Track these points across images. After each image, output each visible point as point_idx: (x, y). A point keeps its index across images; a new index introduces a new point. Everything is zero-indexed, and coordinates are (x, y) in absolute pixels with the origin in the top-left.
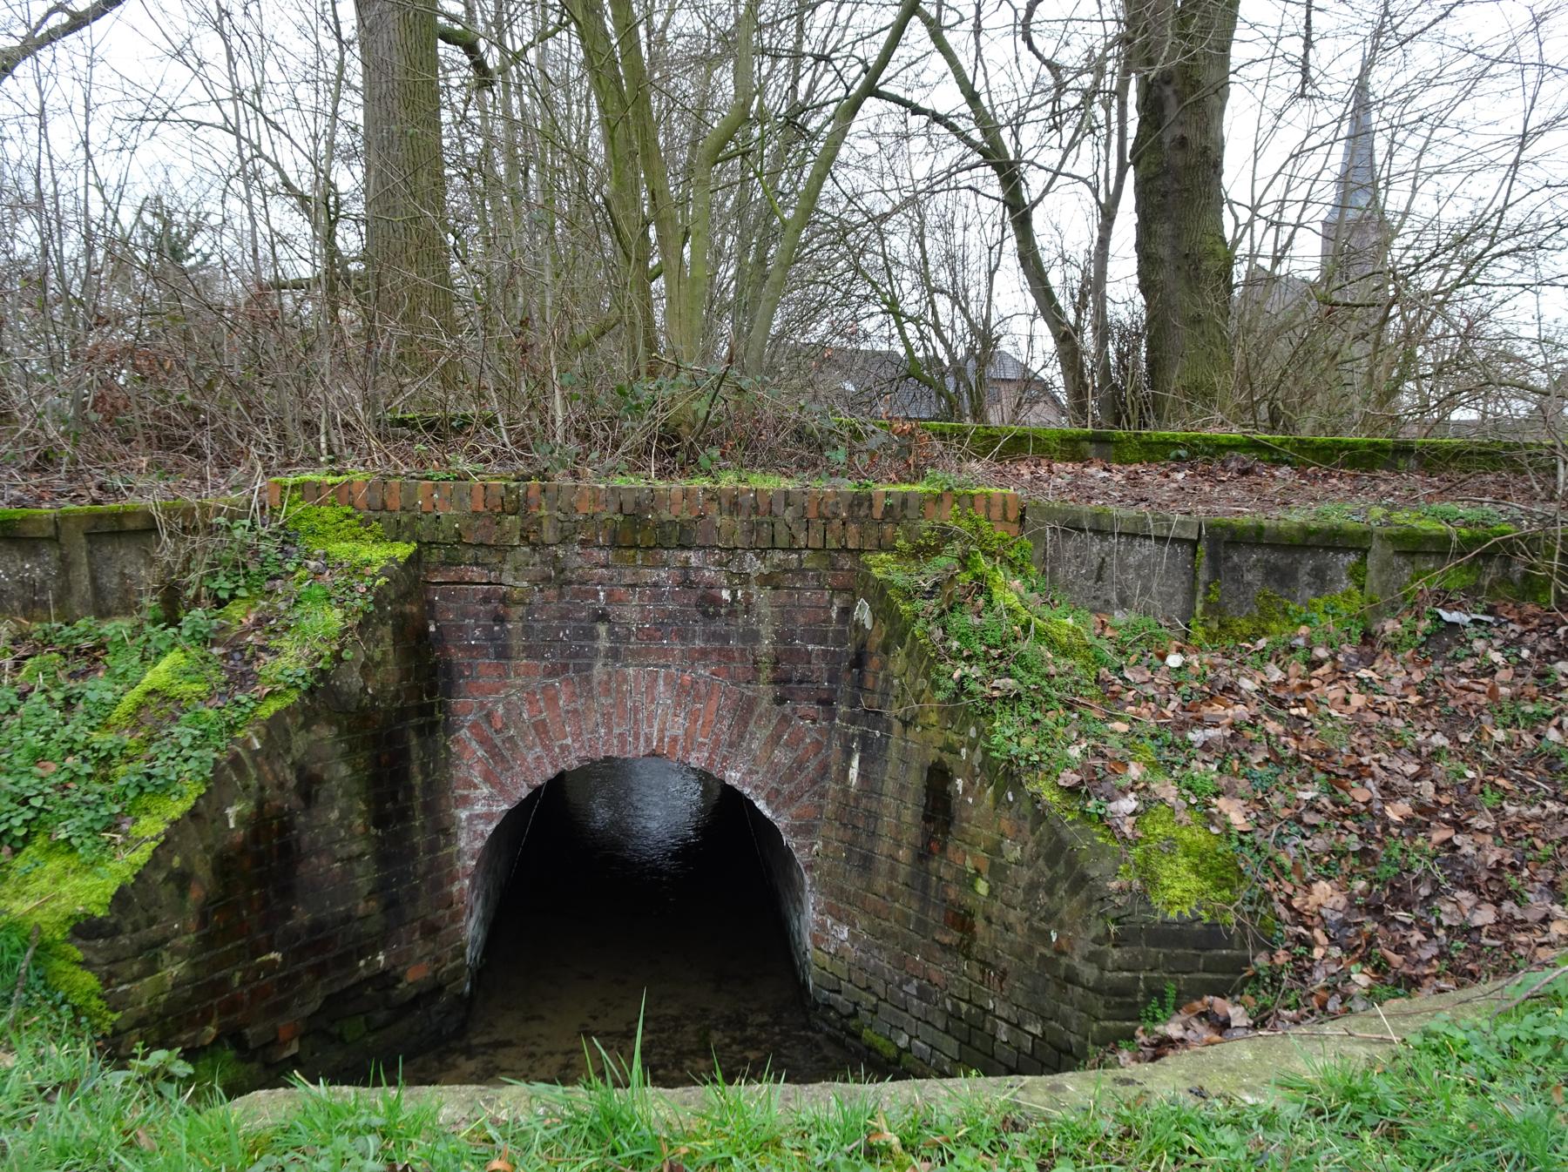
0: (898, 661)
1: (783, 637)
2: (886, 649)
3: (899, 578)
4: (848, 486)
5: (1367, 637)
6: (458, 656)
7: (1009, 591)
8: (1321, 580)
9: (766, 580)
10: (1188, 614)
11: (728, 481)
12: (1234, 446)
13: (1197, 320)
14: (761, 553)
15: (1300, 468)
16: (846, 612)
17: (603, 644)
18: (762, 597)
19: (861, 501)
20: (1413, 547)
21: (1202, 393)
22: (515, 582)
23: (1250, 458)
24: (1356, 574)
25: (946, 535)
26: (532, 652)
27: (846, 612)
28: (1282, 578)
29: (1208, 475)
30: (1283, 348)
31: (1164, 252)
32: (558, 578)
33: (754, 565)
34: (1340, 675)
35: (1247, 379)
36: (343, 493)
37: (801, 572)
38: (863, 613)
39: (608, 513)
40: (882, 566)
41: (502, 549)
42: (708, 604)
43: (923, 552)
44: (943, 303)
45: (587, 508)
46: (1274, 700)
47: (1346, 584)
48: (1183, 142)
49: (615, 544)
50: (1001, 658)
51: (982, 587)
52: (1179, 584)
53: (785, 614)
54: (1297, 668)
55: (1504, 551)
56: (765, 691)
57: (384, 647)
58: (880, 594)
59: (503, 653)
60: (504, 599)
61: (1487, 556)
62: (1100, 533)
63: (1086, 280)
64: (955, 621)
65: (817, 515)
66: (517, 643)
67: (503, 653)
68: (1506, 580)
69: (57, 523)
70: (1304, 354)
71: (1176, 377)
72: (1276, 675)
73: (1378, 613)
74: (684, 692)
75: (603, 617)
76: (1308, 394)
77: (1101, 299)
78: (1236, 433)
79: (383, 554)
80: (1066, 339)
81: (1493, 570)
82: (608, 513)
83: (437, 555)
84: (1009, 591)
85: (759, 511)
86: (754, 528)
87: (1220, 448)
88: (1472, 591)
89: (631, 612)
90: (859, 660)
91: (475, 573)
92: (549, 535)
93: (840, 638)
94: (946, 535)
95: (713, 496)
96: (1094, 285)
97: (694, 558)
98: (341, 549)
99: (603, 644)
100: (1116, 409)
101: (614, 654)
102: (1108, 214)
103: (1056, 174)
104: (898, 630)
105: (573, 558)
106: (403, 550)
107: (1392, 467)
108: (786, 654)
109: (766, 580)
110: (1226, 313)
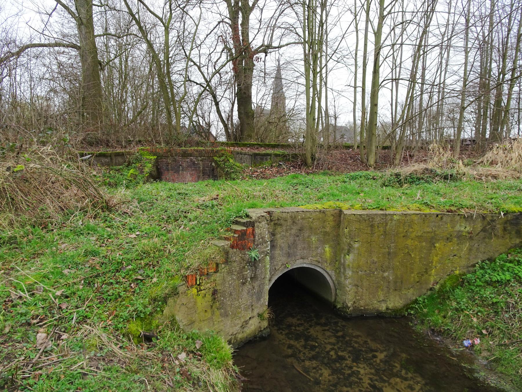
0: (219, 169)
1: (203, 168)
2: (217, 168)
3: (218, 159)
4: (210, 149)
5: (272, 166)
6: (162, 171)
7: (231, 161)
8: (266, 160)
9: (201, 160)
10: (251, 164)
11: (196, 148)
12: (256, 144)
13: (249, 124)
14: (200, 157)
15: (265, 148)
16: (211, 164)
17: (181, 169)
18: (200, 162)
19: (213, 150)
20: (277, 155)
21: (250, 136)
22: (169, 161)
23: (258, 146)
24: (270, 159)
25: (223, 154)
26: (172, 170)
27: (211, 164)
28: (262, 159)
29: (252, 149)
30: (263, 128)
31: (243, 112)
32: (175, 160)
33: (200, 159)
34: (268, 170)
35: (257, 134)
36: (147, 150)
37: (205, 159)
38: (213, 164)
39: (181, 152)
40: (215, 158)
41: (168, 157)
42: (194, 163)
43: (220, 157)
44: (200, 118)
45: (178, 151)
46: (261, 172)
47: (269, 160)
48: (245, 93)
49: (182, 156)
50: (231, 168)
51: (228, 160)
52: (250, 160)
53: (203, 165)
54: (264, 169)
55: (285, 156)
56: (201, 174)
57: (155, 169)
58: (216, 162)
59: (168, 170)
60: (168, 163)
61: (284, 156)
62: (241, 154)
63: (229, 116)
64: (226, 164)
65: (207, 152)
66: (170, 169)
67: (168, 170)
68: (287, 159)
69: (111, 154)
70: (266, 130)
71: (246, 133)
72: (261, 170)
73: (273, 163)
74: (191, 175)
75: (181, 165)
76: (267, 137)
77: (232, 119)
78: (256, 143)
79: (153, 158)
80: (225, 126)
81: (285, 158)
82: (181, 152)
83: (159, 158)
84: (231, 161)
85: (200, 151)
86: (200, 154)
87: (254, 145)
88: (283, 160)
89: (184, 165)
90: (213, 170)
91: (164, 160)
92: (174, 155)
93: (210, 168)
94: (223, 154)
95: (194, 150)
96: (230, 116)
97: (192, 158)
98: (148, 157)
99: (181, 169)
100: (235, 139)
101: (182, 170)
102: (233, 105)
103: (222, 97)
104: (218, 166)
105: (177, 158)
106: (155, 157)
107: (277, 148)
108: (204, 169)
109: (201, 160)
110: (253, 123)
